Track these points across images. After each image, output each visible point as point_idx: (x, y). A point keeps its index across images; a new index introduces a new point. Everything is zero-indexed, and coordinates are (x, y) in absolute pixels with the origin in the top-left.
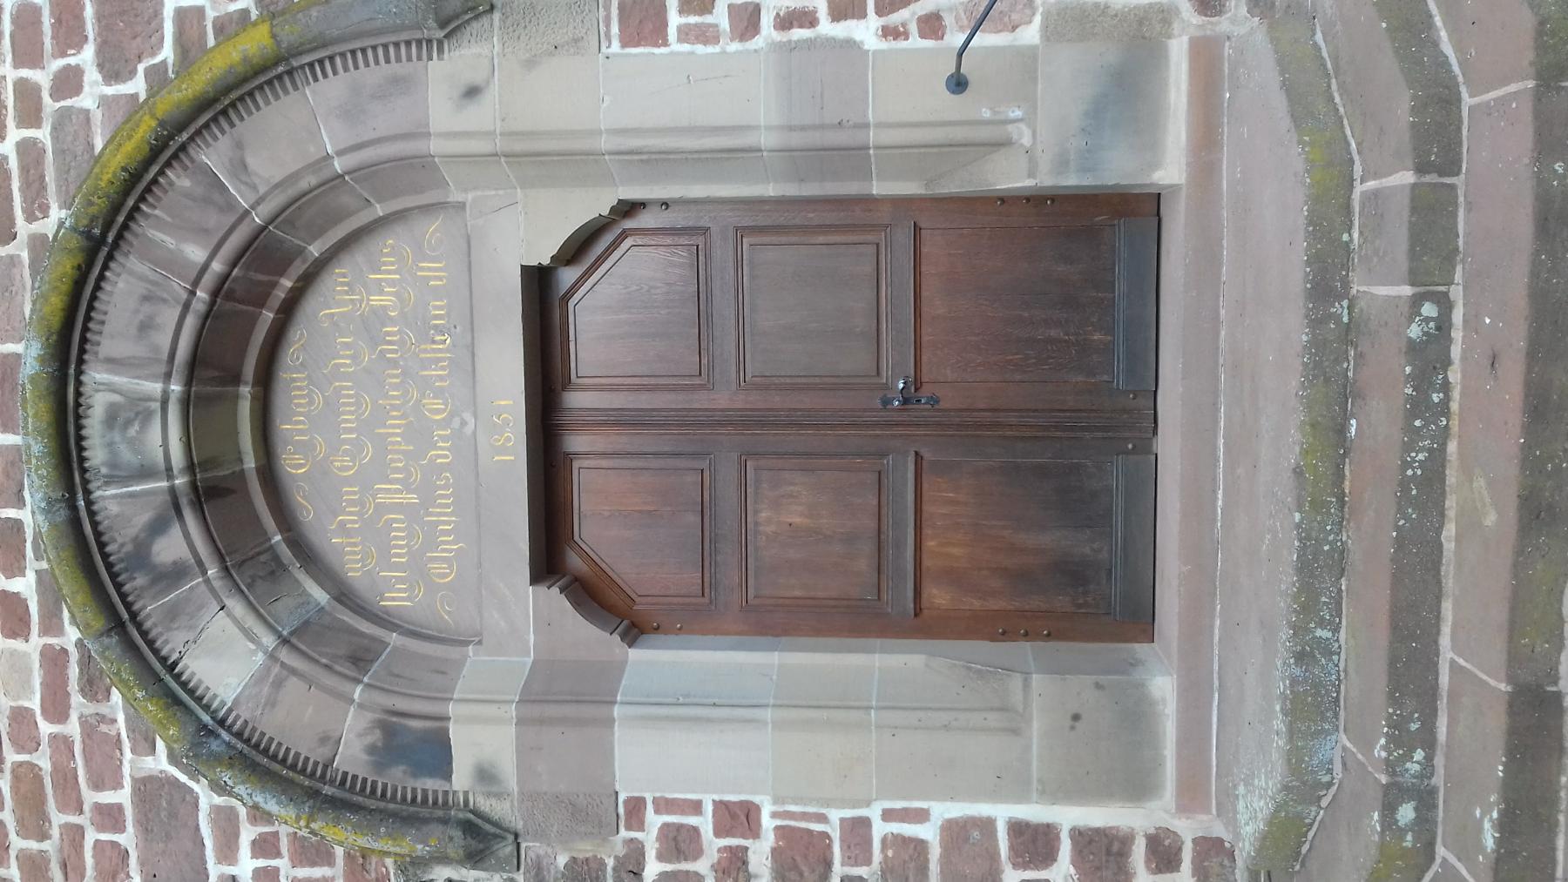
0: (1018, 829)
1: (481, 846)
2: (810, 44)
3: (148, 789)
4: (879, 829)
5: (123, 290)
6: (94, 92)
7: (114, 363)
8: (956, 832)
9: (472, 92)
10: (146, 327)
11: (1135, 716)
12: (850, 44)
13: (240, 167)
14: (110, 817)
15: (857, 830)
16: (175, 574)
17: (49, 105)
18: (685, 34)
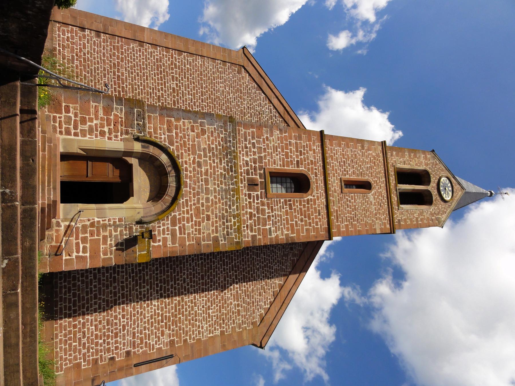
0: (78, 136)
1: (134, 162)
2: (102, 218)
3: (172, 145)
4: (94, 137)
5: (173, 195)
6: (177, 214)
7: (173, 187)
8: (85, 136)
9: (138, 213)
10: (172, 190)
11: (64, 147)
12: (98, 218)
13: (162, 206)
14: (177, 142)
15: (96, 137)
16: (169, 166)
17: (181, 212)
18: (116, 219)
